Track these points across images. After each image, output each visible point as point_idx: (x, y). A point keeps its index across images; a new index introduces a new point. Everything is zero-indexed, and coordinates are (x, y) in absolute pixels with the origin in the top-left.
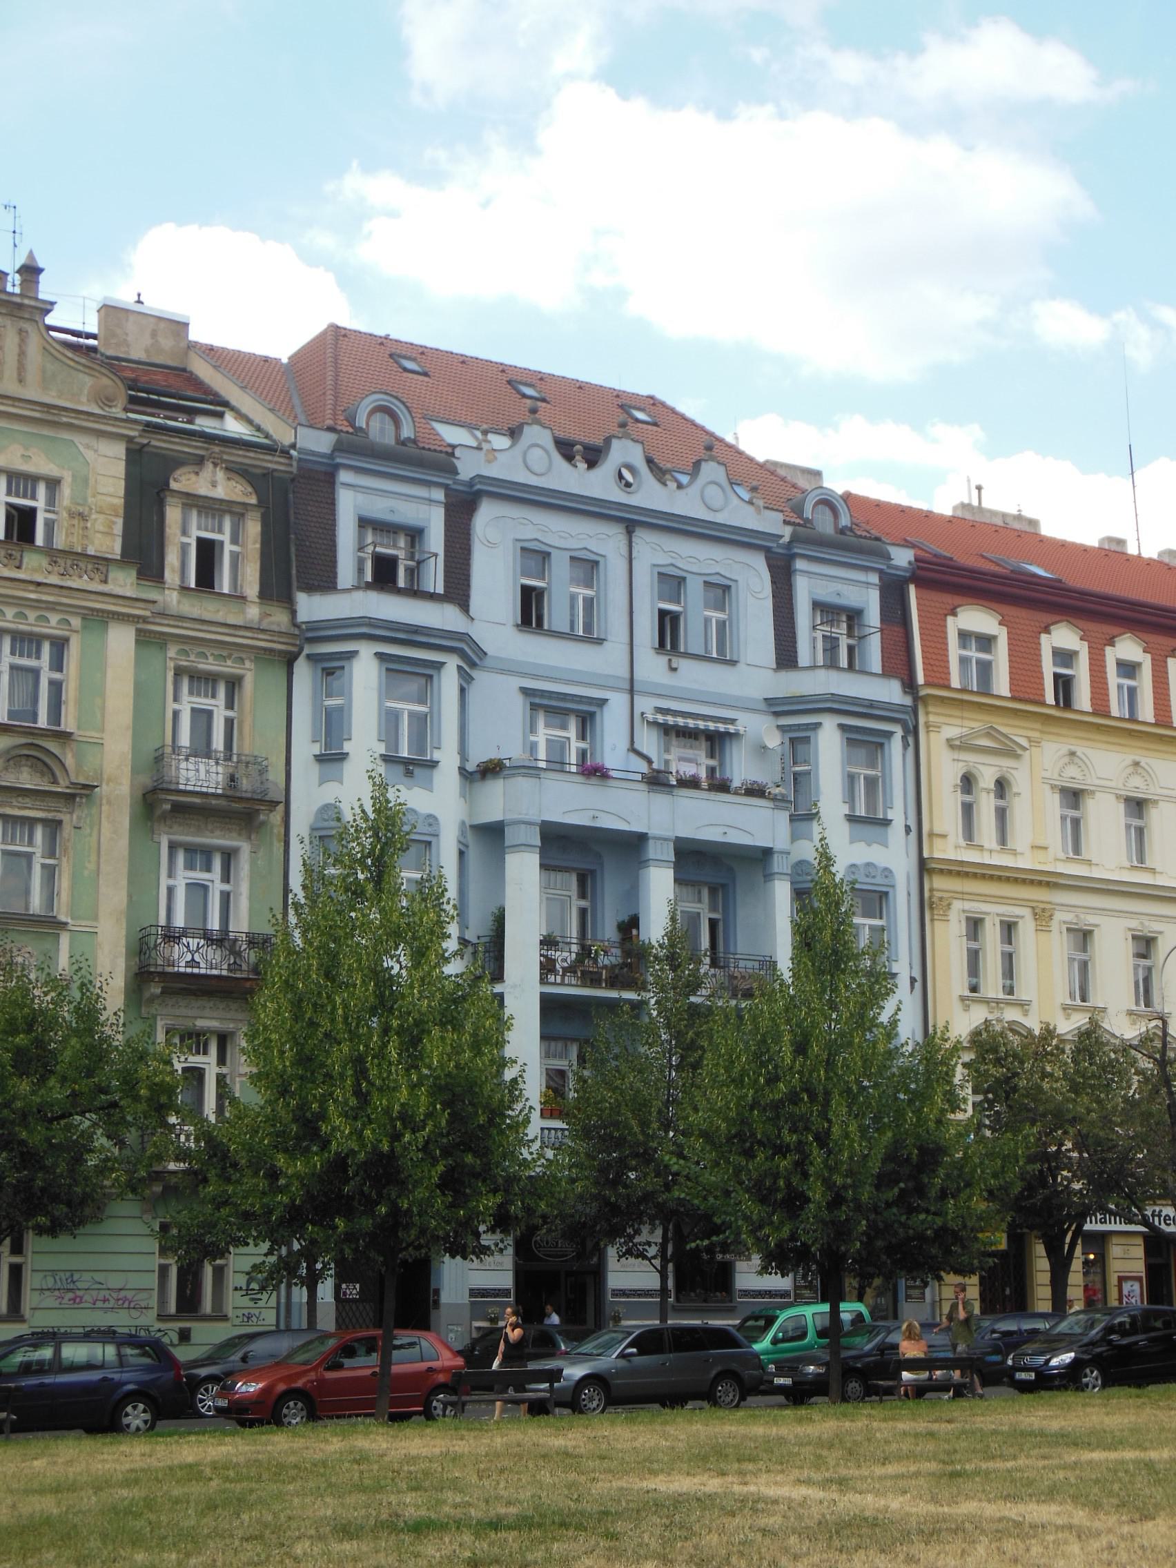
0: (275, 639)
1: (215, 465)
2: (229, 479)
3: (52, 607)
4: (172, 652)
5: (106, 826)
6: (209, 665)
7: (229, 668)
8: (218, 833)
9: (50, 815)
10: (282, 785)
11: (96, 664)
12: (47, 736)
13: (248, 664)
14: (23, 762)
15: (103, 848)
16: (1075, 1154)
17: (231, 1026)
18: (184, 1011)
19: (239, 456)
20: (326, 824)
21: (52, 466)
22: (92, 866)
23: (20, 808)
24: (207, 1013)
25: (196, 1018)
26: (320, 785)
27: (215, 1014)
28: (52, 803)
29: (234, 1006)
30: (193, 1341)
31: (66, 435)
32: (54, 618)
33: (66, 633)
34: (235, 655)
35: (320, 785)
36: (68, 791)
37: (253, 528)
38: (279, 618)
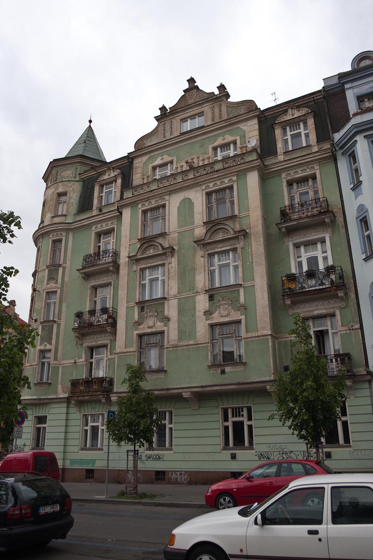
0: (325, 152)
1: (292, 108)
2: (299, 111)
3: (225, 176)
4: (283, 175)
5: (253, 243)
6: (300, 174)
7: (308, 172)
8: (313, 234)
9: (232, 247)
10: (340, 206)
11: (244, 189)
12: (228, 220)
13: (316, 168)
14: (220, 231)
15: (253, 253)
16: (297, 408)
17: (331, 310)
18: (309, 309)
19: (302, 101)
20: (360, 214)
21: (232, 137)
22: (250, 260)
23: (221, 248)
24: (320, 307)
25: (314, 311)
26: (191, 81)
27: (323, 307)
28: (232, 242)
29: (332, 302)
30: (333, 457)
31: (236, 126)
32: (226, 181)
33: (232, 183)
34: (310, 166)
35: (191, 81)
36: (234, 236)
37: (311, 122)
38: (327, 146)
